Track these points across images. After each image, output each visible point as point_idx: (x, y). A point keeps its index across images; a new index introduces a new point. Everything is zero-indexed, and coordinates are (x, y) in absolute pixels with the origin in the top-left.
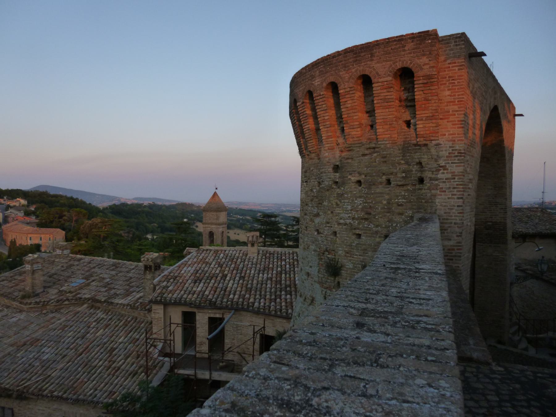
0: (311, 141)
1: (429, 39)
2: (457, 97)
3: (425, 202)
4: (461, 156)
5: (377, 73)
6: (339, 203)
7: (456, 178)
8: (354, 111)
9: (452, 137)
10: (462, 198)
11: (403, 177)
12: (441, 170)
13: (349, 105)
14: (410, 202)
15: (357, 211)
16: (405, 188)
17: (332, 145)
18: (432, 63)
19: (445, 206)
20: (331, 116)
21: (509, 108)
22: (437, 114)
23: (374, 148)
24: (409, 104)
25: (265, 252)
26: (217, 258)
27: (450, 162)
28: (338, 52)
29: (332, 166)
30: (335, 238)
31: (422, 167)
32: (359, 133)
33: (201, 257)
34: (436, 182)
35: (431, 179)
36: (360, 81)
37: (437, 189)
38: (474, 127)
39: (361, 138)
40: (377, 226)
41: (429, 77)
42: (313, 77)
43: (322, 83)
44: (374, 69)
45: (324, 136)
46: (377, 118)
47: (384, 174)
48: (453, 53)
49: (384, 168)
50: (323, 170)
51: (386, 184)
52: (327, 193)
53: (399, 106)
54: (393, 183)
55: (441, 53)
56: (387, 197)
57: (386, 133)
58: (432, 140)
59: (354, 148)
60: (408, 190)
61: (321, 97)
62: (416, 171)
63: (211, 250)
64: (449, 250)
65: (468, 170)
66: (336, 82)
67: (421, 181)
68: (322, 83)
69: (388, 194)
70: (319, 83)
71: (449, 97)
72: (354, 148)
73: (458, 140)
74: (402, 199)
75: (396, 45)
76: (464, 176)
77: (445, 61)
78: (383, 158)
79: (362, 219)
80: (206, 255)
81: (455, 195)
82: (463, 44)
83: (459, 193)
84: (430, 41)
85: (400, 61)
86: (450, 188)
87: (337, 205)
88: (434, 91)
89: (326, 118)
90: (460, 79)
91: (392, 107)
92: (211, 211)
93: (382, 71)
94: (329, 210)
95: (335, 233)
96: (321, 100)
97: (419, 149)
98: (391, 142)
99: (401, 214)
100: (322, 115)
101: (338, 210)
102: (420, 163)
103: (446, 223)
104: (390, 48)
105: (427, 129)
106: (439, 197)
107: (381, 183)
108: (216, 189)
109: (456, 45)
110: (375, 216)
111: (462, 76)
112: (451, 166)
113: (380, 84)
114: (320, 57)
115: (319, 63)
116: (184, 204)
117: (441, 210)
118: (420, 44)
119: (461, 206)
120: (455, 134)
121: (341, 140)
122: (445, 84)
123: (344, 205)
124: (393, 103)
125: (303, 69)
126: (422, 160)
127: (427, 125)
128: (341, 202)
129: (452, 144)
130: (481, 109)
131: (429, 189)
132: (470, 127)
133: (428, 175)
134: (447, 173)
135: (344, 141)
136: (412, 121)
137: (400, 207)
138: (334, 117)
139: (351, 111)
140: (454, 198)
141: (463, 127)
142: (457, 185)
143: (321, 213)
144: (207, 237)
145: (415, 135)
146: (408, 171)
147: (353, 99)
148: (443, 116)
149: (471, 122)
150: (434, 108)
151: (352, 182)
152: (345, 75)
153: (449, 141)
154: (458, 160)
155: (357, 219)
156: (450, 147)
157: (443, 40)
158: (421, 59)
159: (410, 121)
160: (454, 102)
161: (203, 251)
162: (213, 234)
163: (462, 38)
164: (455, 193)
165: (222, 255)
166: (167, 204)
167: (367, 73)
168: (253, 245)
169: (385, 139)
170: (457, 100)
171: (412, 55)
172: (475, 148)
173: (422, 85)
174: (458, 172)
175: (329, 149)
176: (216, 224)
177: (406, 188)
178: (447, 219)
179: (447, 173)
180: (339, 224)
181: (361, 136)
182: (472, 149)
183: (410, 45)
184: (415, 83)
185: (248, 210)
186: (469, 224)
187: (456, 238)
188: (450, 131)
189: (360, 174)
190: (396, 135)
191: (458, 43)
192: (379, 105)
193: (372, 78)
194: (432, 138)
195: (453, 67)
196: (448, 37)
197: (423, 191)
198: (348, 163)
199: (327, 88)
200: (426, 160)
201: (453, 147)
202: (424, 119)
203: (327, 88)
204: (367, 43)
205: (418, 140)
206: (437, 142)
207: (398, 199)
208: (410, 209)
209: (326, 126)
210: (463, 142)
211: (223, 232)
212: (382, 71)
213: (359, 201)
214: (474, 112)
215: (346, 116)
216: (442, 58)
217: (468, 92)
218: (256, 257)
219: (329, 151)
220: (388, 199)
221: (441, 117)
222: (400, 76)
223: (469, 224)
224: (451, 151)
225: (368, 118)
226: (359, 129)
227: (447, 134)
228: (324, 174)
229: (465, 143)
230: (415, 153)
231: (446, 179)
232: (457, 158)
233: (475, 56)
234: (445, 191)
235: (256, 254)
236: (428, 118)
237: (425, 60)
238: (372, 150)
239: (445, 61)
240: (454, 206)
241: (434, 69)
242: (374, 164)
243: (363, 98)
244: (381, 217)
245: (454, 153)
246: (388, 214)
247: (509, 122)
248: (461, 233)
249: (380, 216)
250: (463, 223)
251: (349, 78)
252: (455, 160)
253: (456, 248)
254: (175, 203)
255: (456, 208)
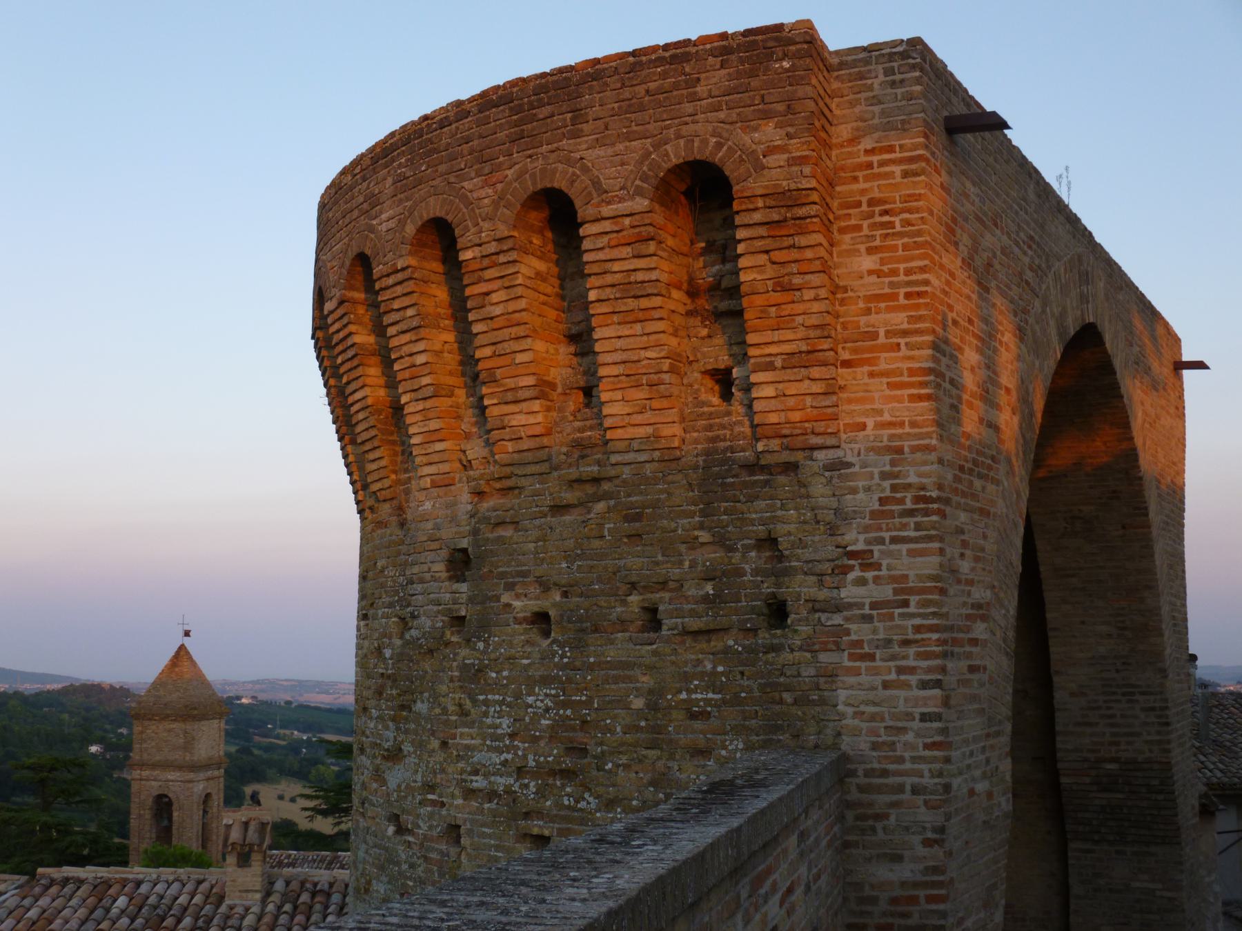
0: (377, 454)
1: (785, 56)
2: (902, 278)
3: (796, 702)
4: (927, 513)
5: (596, 183)
6: (468, 704)
7: (913, 599)
8: (514, 331)
9: (892, 437)
10: (938, 684)
11: (706, 599)
12: (852, 568)
13: (497, 310)
14: (736, 701)
15: (535, 740)
16: (716, 644)
17: (445, 467)
18: (798, 148)
19: (873, 718)
20: (438, 353)
21: (1154, 338)
22: (826, 345)
23: (596, 480)
24: (724, 305)
25: (295, 885)
26: (99, 913)
27: (887, 535)
28: (459, 103)
29: (444, 554)
30: (453, 851)
31: (781, 558)
32: (540, 418)
33: (33, 913)
34: (837, 619)
35: (816, 606)
36: (536, 217)
37: (839, 649)
38: (987, 395)
39: (545, 441)
40: (610, 804)
41: (788, 199)
42: (374, 201)
43: (402, 223)
44: (585, 170)
45: (416, 429)
46: (602, 358)
47: (633, 586)
48: (883, 112)
49: (634, 562)
50: (415, 570)
51: (643, 629)
52: (427, 665)
53: (689, 314)
54: (667, 623)
55: (837, 112)
56: (646, 681)
57: (638, 419)
58: (813, 449)
59: (523, 482)
60: (727, 650)
61: (400, 276)
62: (756, 572)
63: (80, 882)
64: (894, 901)
65: (965, 566)
66: (449, 218)
67: (778, 612)
68: (402, 223)
69: (651, 668)
70: (391, 224)
71: (874, 279)
72: (523, 482)
73: (915, 449)
74: (706, 689)
75: (664, 75)
76: (943, 591)
77: (853, 141)
78: (628, 519)
79: (553, 773)
80: (58, 903)
81: (912, 670)
82: (918, 81)
83: (924, 664)
84: (786, 64)
85: (679, 137)
86: (888, 642)
87: (464, 713)
88: (809, 254)
89: (420, 359)
90: (910, 211)
91: (656, 314)
92: (166, 718)
93: (613, 176)
94: (433, 733)
95: (453, 832)
96: (399, 290)
97: (766, 483)
98: (657, 454)
99: (702, 752)
100: (406, 350)
101: (465, 737)
102: (770, 542)
103: (879, 789)
104: (641, 90)
105: (791, 402)
106: (852, 680)
107: (622, 624)
108: (187, 634)
109: (893, 84)
110: (602, 757)
111: (918, 197)
112: (890, 554)
113: (607, 226)
114: (396, 126)
115: (394, 147)
116: (91, 690)
117: (856, 732)
118: (753, 74)
119: (938, 717)
120: (902, 424)
121: (475, 450)
122: (858, 228)
123: (486, 714)
124: (657, 301)
125: (344, 172)
126: (781, 529)
127: (792, 389)
128: (474, 702)
129: (893, 463)
130: (1021, 333)
131: (808, 646)
132: (965, 397)
133: (801, 588)
134: (877, 580)
135: (485, 452)
136: (736, 372)
137: (698, 725)
138: (451, 359)
139: (505, 334)
140: (906, 685)
141: (928, 397)
142: (918, 629)
143: (407, 748)
144: (148, 815)
145: (747, 430)
146: (724, 573)
147: (516, 286)
148: (855, 351)
149: (969, 381)
150: (814, 320)
151: (518, 621)
152: (482, 193)
153: (878, 451)
154: (918, 527)
155: (535, 775)
156: (884, 476)
157: (842, 65)
158: (756, 129)
159: (728, 371)
160: (894, 297)
161: (47, 888)
162: (170, 804)
163: (914, 57)
164: (911, 663)
165: (122, 901)
166: (29, 688)
167: (559, 183)
168: (244, 860)
169: (635, 445)
170: (902, 291)
171: (722, 115)
172: (997, 482)
173: (762, 231)
174: (919, 577)
175: (435, 485)
176: (180, 768)
177: (720, 645)
178: (885, 773)
179: (877, 580)
180: (469, 793)
181: (548, 433)
182: (978, 484)
183: (716, 79)
184: (738, 220)
185: (329, 710)
186: (981, 787)
187: (921, 851)
188: (880, 412)
189: (545, 586)
190: (677, 429)
191: (898, 77)
192: (604, 308)
193: (578, 203)
194: (815, 440)
195: (882, 164)
196: (862, 55)
197: (786, 656)
198: (500, 540)
199: (418, 244)
200: (792, 528)
201: (896, 476)
202: (778, 362)
203: (418, 244)
204: (561, 70)
205: (760, 447)
206: (831, 454)
207: (689, 691)
208: (738, 730)
209: (420, 395)
210: (933, 457)
211: (208, 796)
212: (613, 176)
213: (538, 699)
214: (987, 343)
215: (487, 351)
216: (843, 132)
217: (952, 261)
218: (256, 909)
219: (435, 492)
220: (651, 692)
221: (846, 356)
222: (688, 194)
223: (981, 787)
224: (888, 493)
225: (575, 360)
226: (536, 405)
227: (870, 423)
228: (419, 587)
229: (940, 461)
230: (751, 499)
231: (874, 606)
232: (912, 521)
233: (971, 129)
234: (872, 657)
235: (258, 896)
236: (795, 361)
237: (770, 132)
238: (590, 489)
239: (853, 141)
240: (909, 716)
241: (807, 170)
242: (596, 543)
243: (556, 282)
244: (627, 767)
245: (901, 501)
246: (653, 754)
247: (1155, 386)
248: (942, 830)
249: (624, 760)
250: (947, 788)
251: (496, 204)
252: (904, 527)
253: (922, 893)
254: (56, 686)
255: (916, 724)
